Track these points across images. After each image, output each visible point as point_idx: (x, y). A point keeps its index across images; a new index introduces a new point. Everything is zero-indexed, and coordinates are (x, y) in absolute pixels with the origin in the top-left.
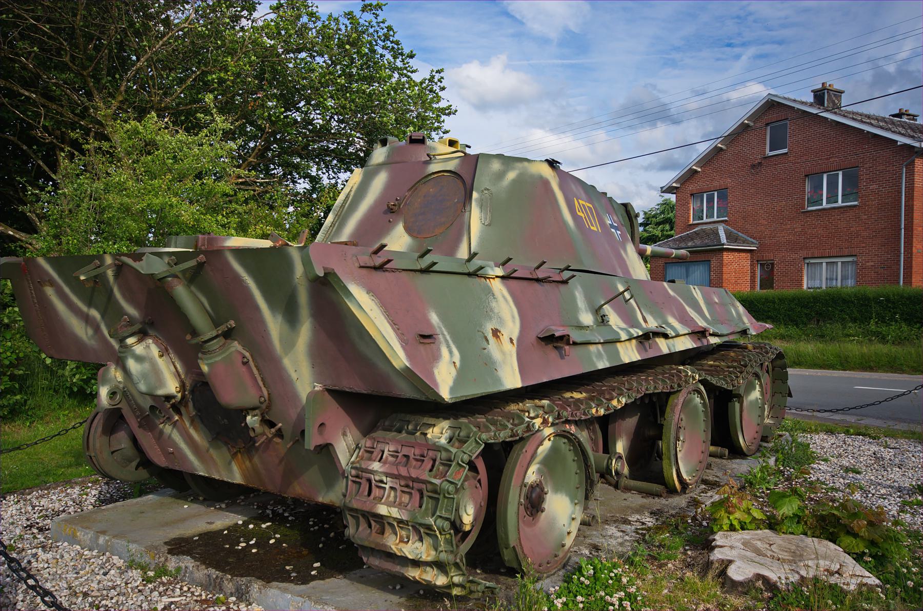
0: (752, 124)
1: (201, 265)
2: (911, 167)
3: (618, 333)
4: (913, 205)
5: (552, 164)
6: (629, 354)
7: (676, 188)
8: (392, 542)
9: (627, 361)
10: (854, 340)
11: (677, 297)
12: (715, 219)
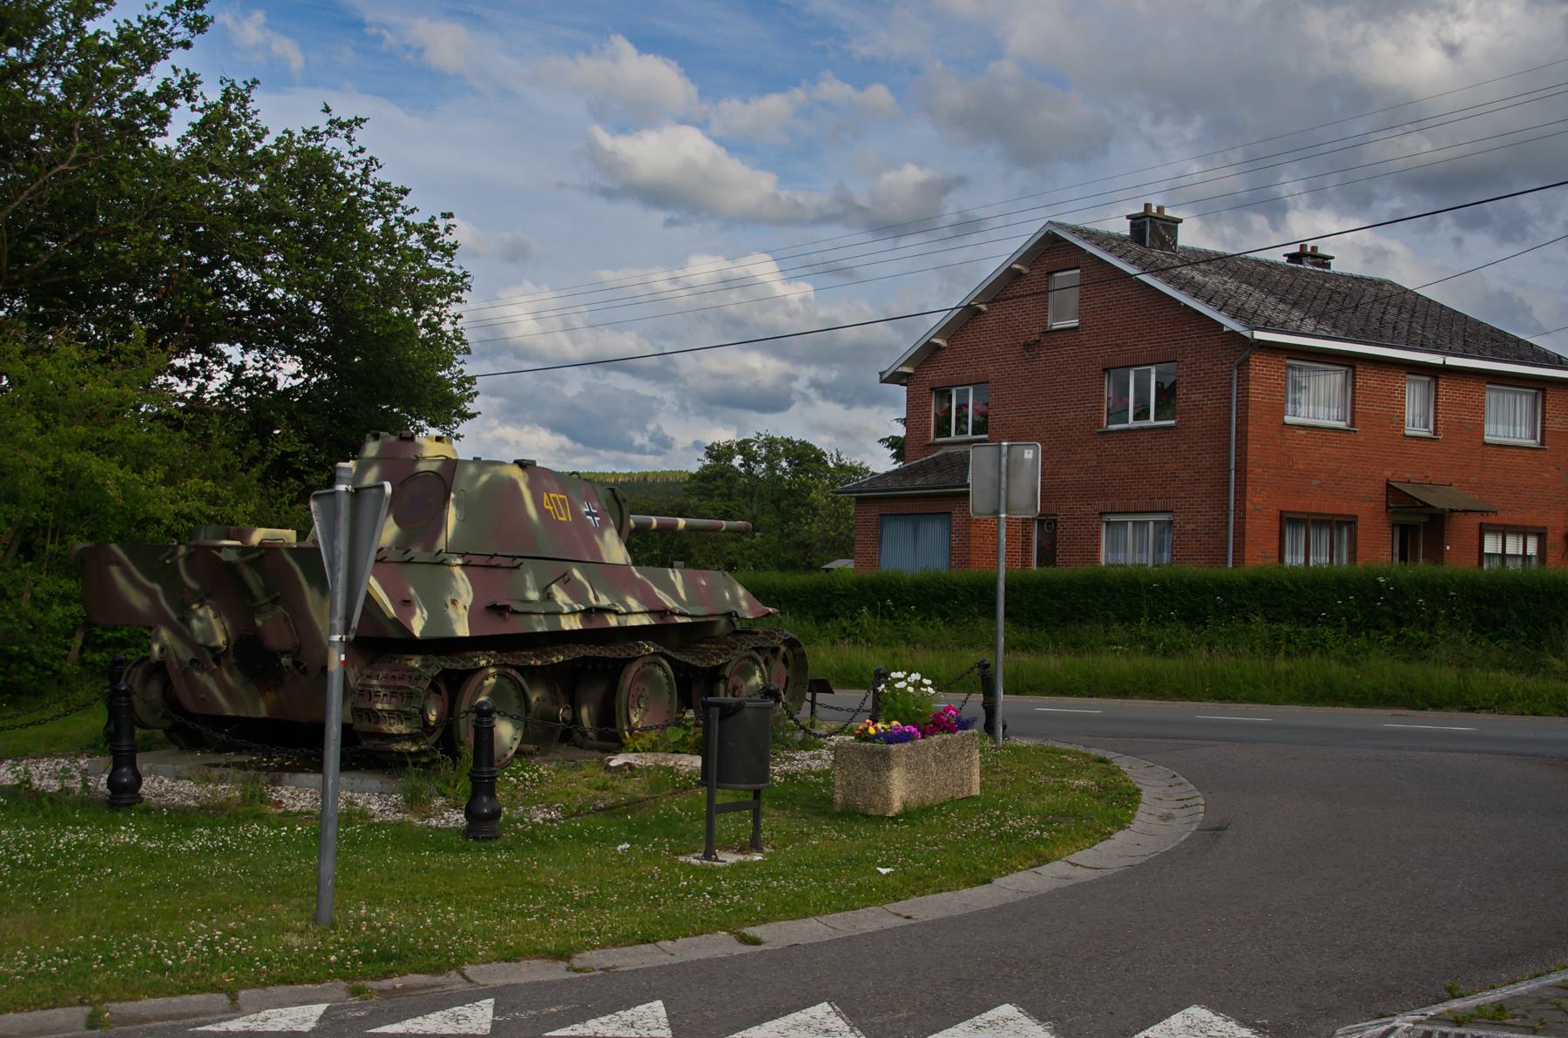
0: (1025, 270)
1: (262, 556)
2: (1244, 365)
3: (561, 607)
4: (1247, 432)
5: (521, 464)
6: (571, 624)
7: (908, 375)
8: (385, 728)
9: (567, 628)
10: (1116, 651)
11: (645, 579)
12: (970, 436)
